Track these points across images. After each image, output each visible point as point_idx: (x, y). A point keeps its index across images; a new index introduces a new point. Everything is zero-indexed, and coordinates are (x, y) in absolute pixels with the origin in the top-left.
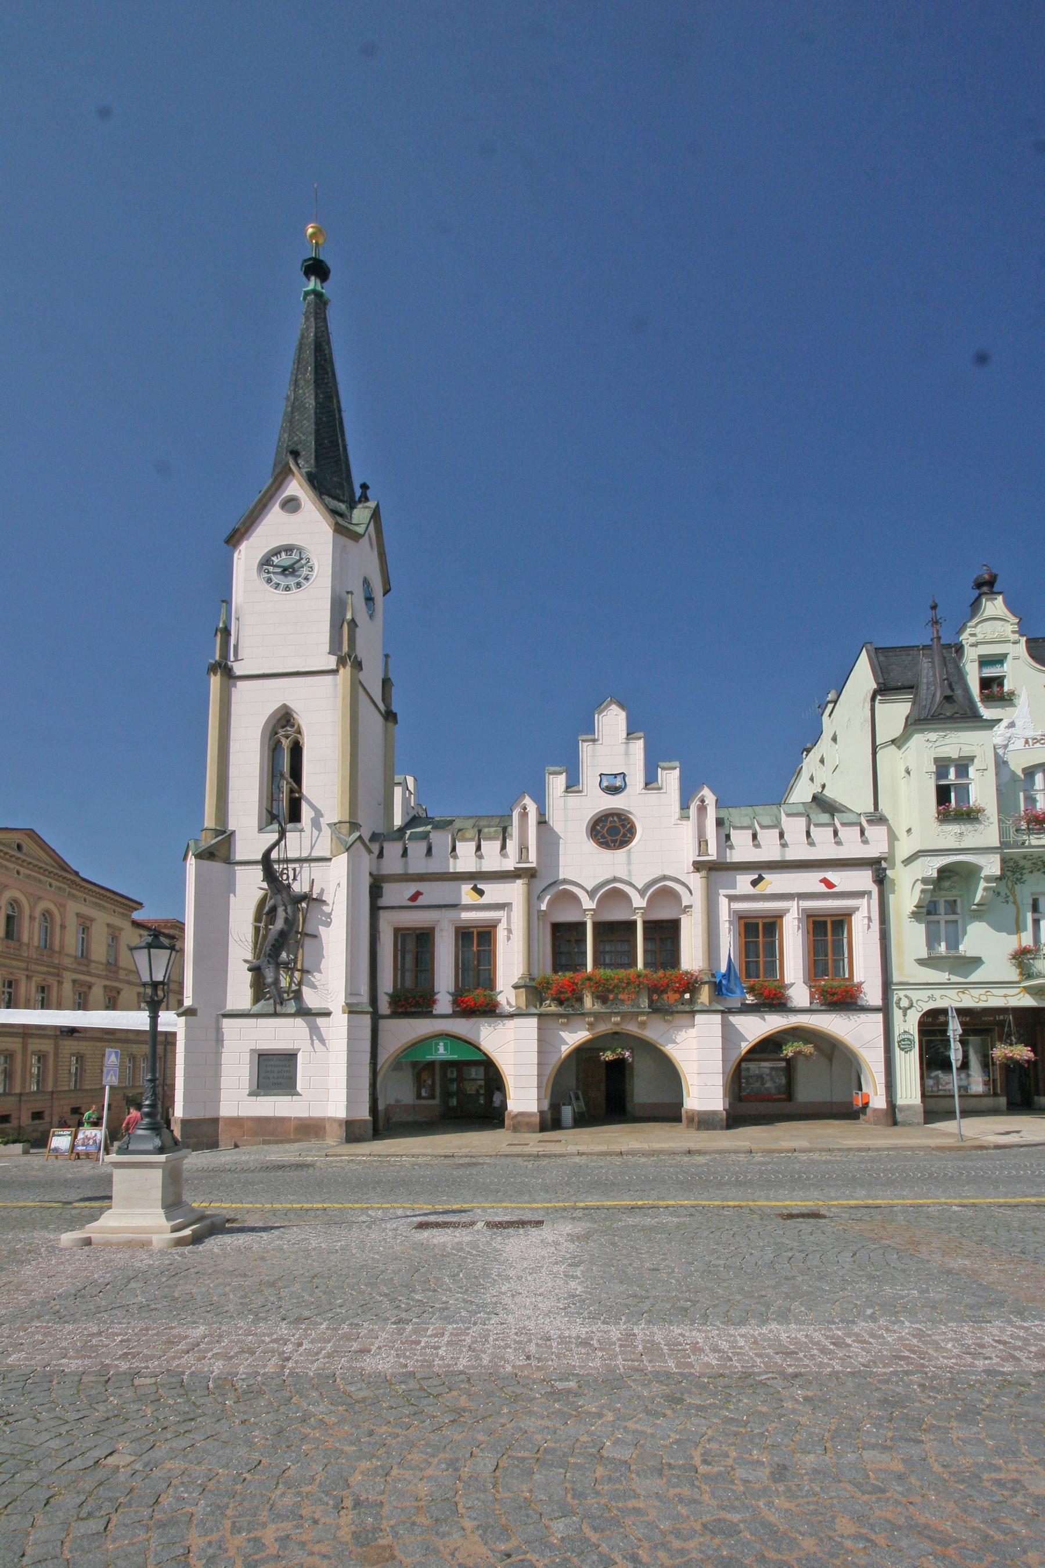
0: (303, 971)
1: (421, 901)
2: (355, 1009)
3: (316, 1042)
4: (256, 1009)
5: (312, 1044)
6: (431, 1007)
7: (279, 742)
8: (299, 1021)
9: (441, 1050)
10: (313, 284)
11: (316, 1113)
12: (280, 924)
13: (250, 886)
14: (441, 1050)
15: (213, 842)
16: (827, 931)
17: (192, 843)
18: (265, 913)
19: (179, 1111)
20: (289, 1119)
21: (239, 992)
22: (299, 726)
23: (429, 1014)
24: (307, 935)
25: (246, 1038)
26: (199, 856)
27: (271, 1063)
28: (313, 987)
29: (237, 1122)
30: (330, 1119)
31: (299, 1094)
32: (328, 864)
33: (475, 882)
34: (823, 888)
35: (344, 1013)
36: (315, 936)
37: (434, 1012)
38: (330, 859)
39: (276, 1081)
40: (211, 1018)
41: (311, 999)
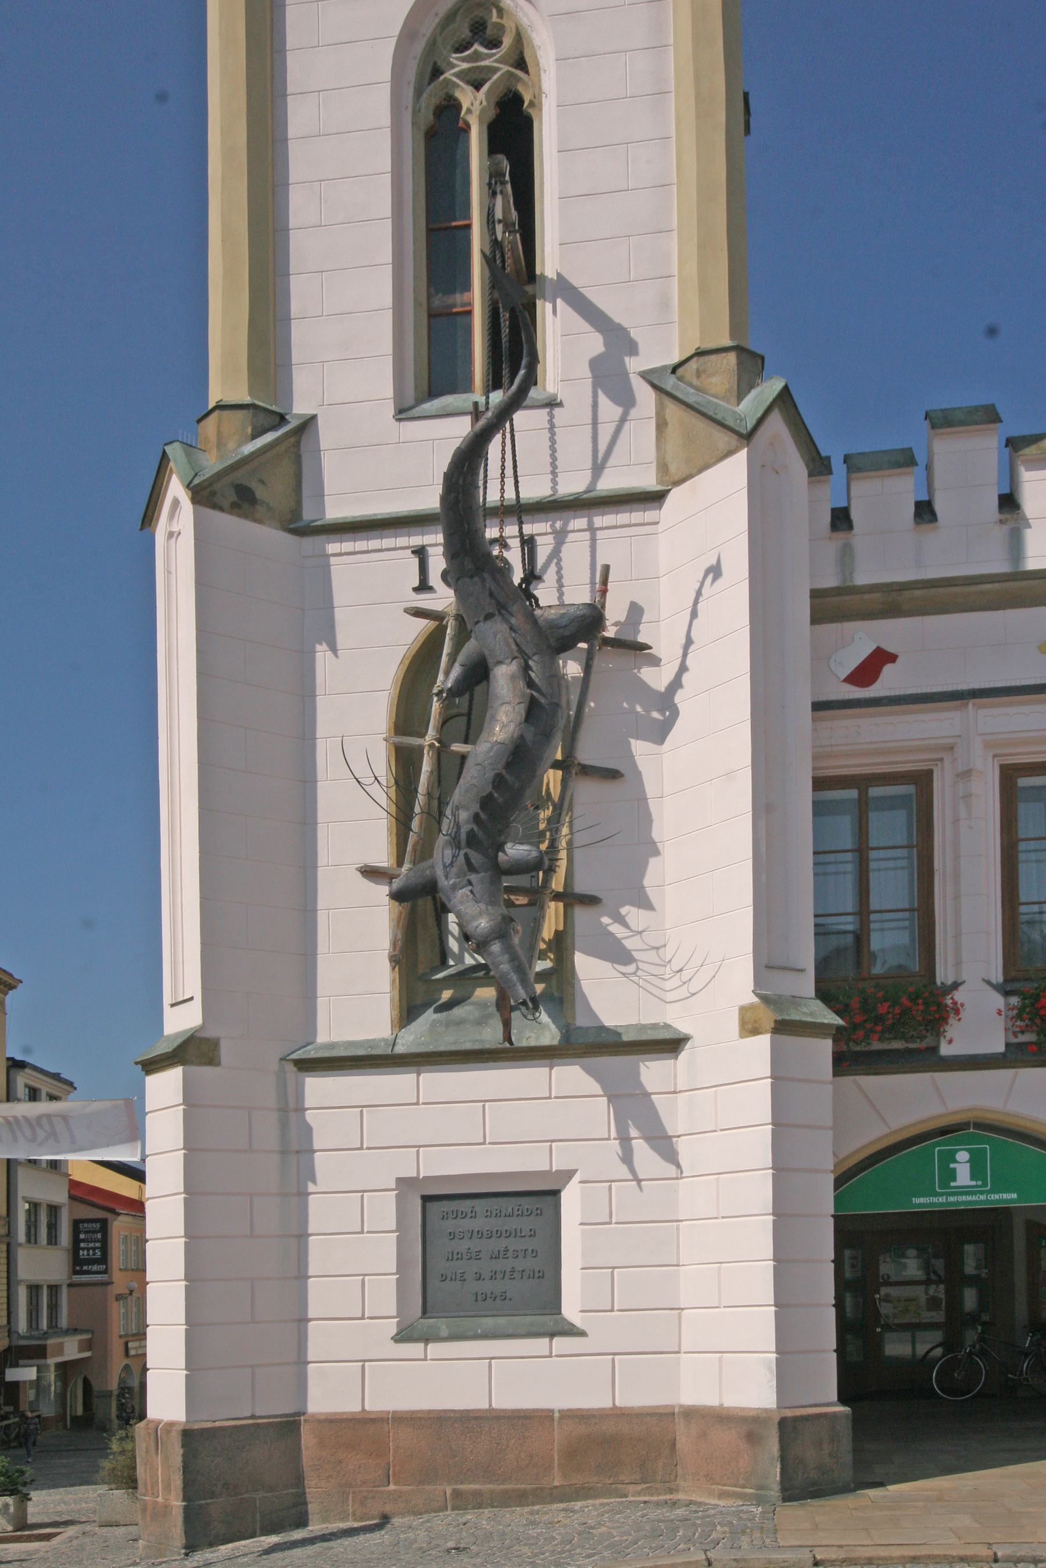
0: (570, 898)
1: (890, 682)
2: (795, 1016)
3: (640, 1146)
4: (410, 1039)
5: (627, 1158)
6: (938, 1034)
7: (449, 108)
8: (571, 1076)
9: (963, 1175)
11: (638, 1393)
12: (504, 723)
13: (379, 608)
14: (963, 1175)
15: (249, 448)
17: (175, 451)
18: (437, 694)
19: (166, 1399)
20: (541, 1418)
21: (355, 988)
22: (519, 38)
23: (929, 1060)
24: (587, 771)
25: (388, 1137)
26: (202, 494)
27: (467, 1224)
28: (617, 954)
29: (362, 1431)
30: (690, 1413)
31: (572, 1331)
32: (650, 515)
35: (749, 1028)
36: (612, 775)
37: (945, 1050)
38: (656, 498)
39: (487, 1286)
40: (261, 1065)
41: (607, 994)
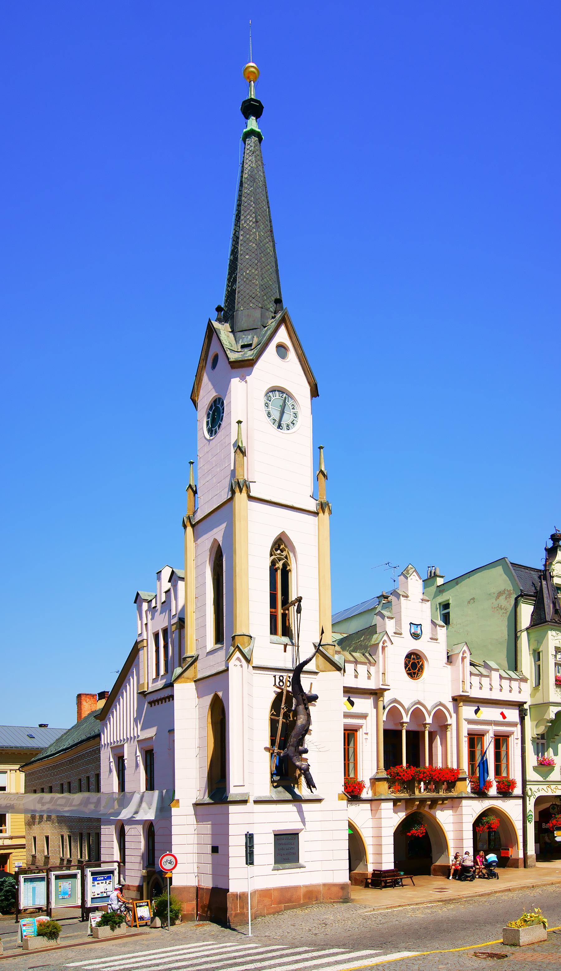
10: (252, 124)
16: (501, 741)
33: (350, 695)
34: (500, 718)
